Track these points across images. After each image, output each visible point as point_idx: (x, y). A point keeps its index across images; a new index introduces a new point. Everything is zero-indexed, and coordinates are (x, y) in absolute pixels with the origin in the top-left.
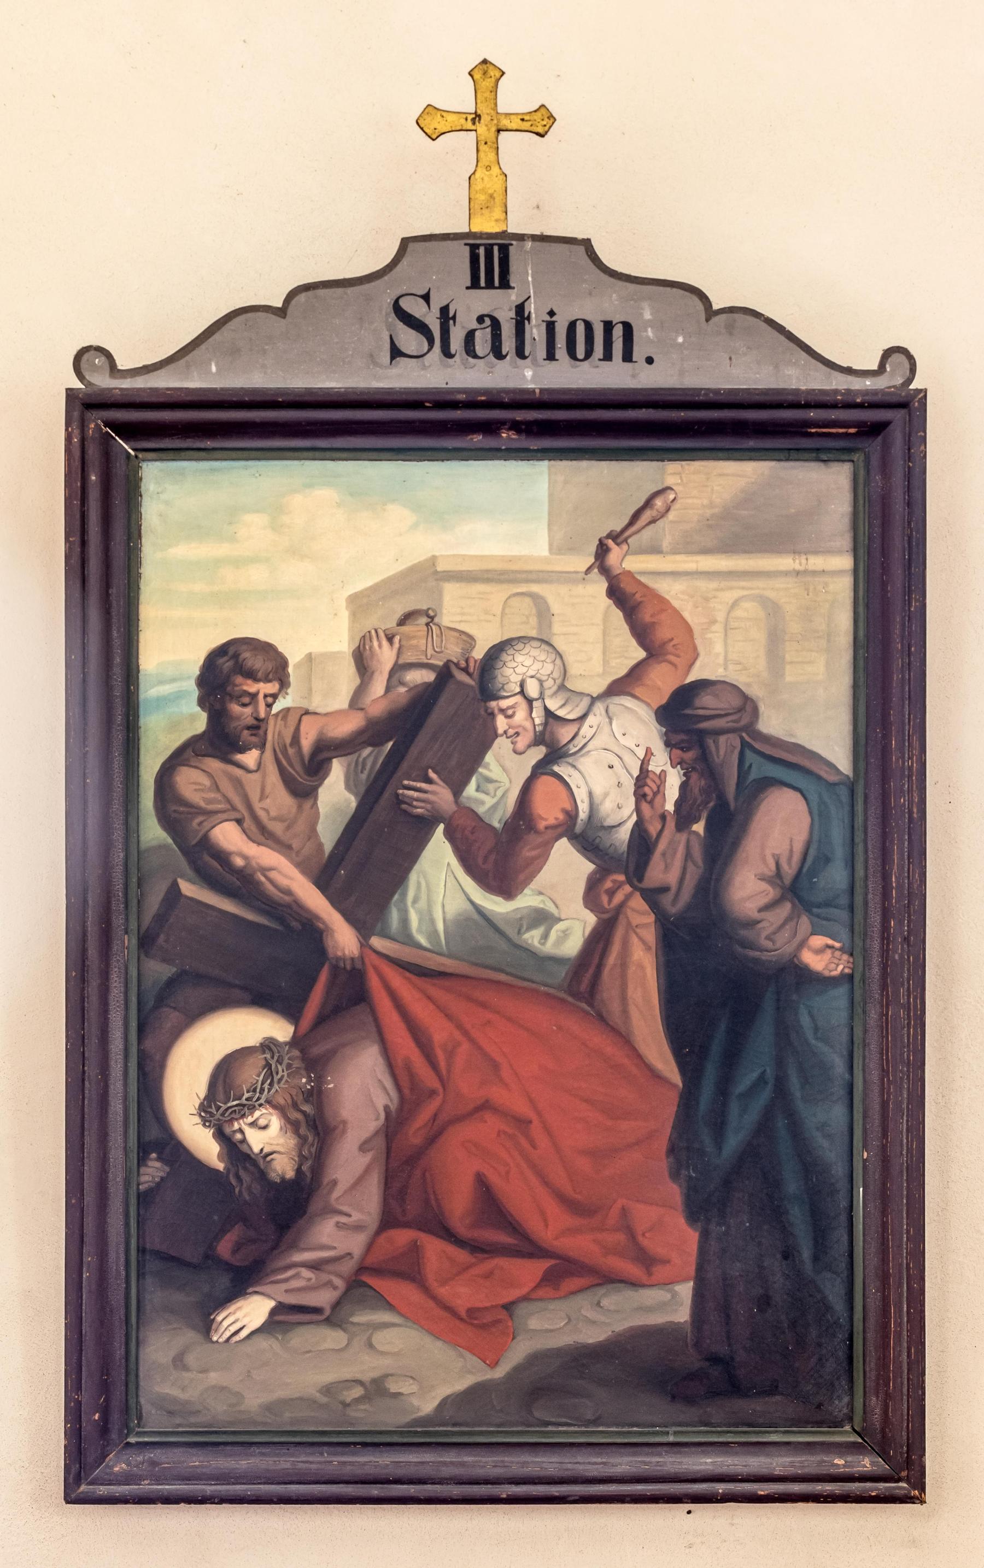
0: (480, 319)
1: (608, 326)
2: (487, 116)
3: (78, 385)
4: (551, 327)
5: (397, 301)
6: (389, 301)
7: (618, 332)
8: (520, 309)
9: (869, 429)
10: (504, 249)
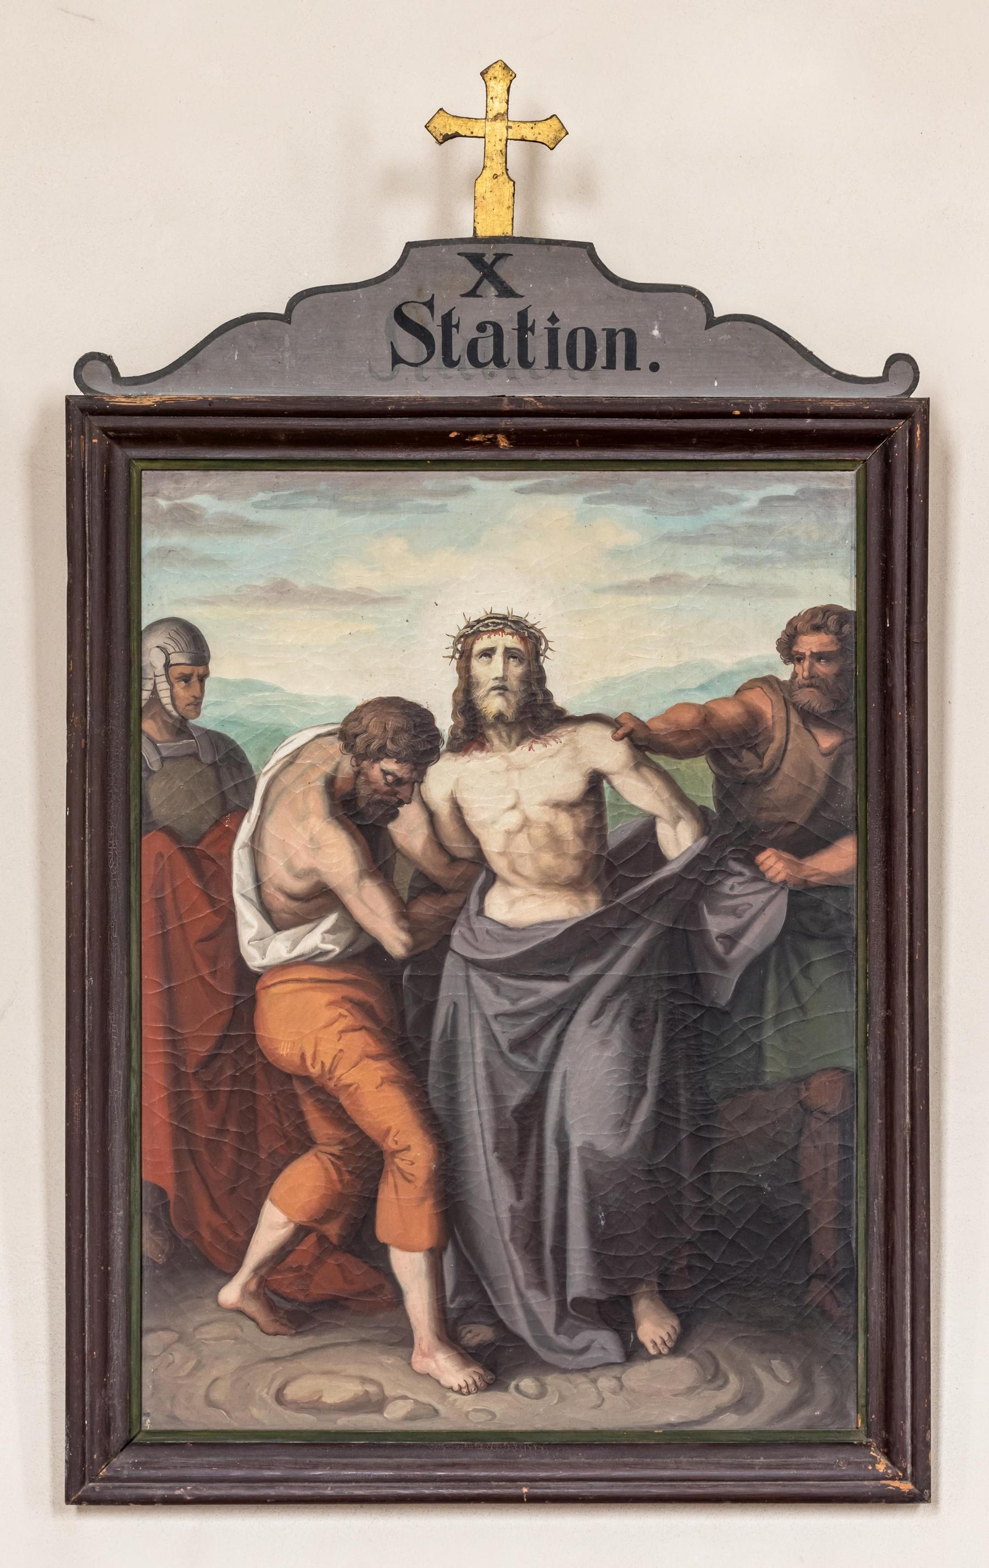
0: (481, 327)
3: (77, 392)
4: (553, 335)
8: (523, 316)
9: (874, 442)
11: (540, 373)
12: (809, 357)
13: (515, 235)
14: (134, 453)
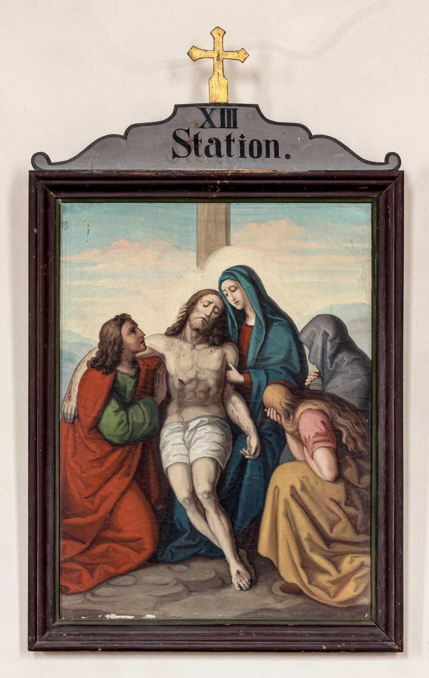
0: (210, 141)
1: (268, 142)
3: (33, 169)
4: (242, 144)
5: (174, 133)
6: (173, 130)
7: (272, 145)
9: (379, 188)
10: (235, 110)
13: (229, 103)
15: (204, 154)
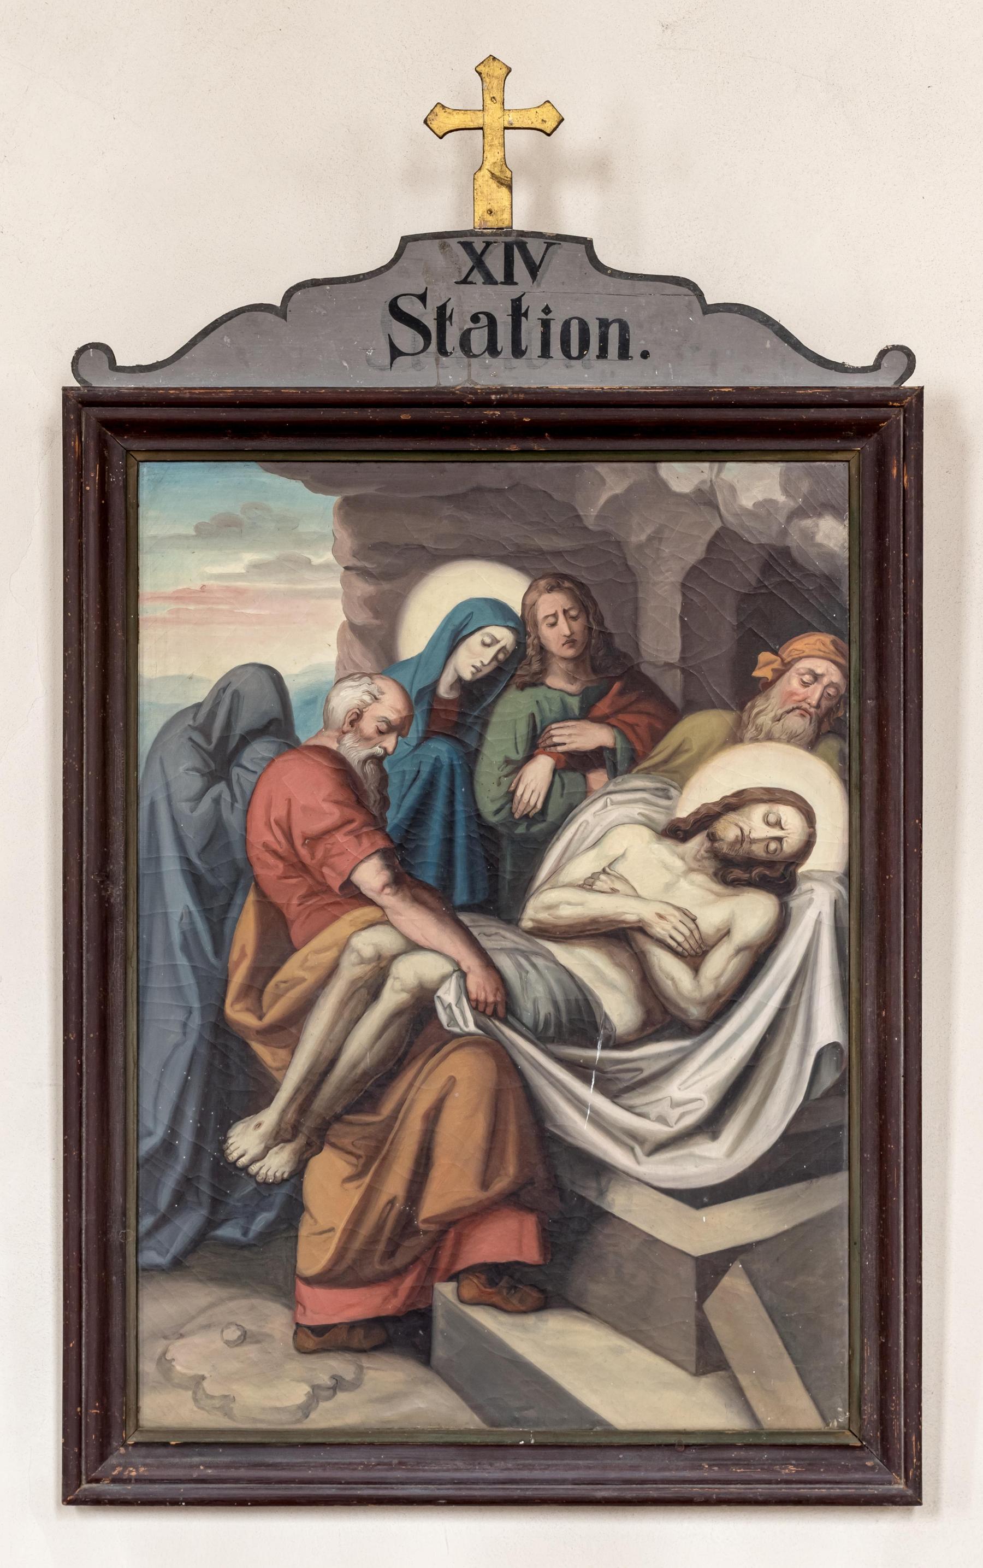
0: (475, 318)
1: (604, 324)
2: (486, 116)
3: (76, 384)
4: (546, 324)
7: (614, 331)
11: (535, 362)
12: (797, 346)
14: (135, 444)
15: (458, 349)
